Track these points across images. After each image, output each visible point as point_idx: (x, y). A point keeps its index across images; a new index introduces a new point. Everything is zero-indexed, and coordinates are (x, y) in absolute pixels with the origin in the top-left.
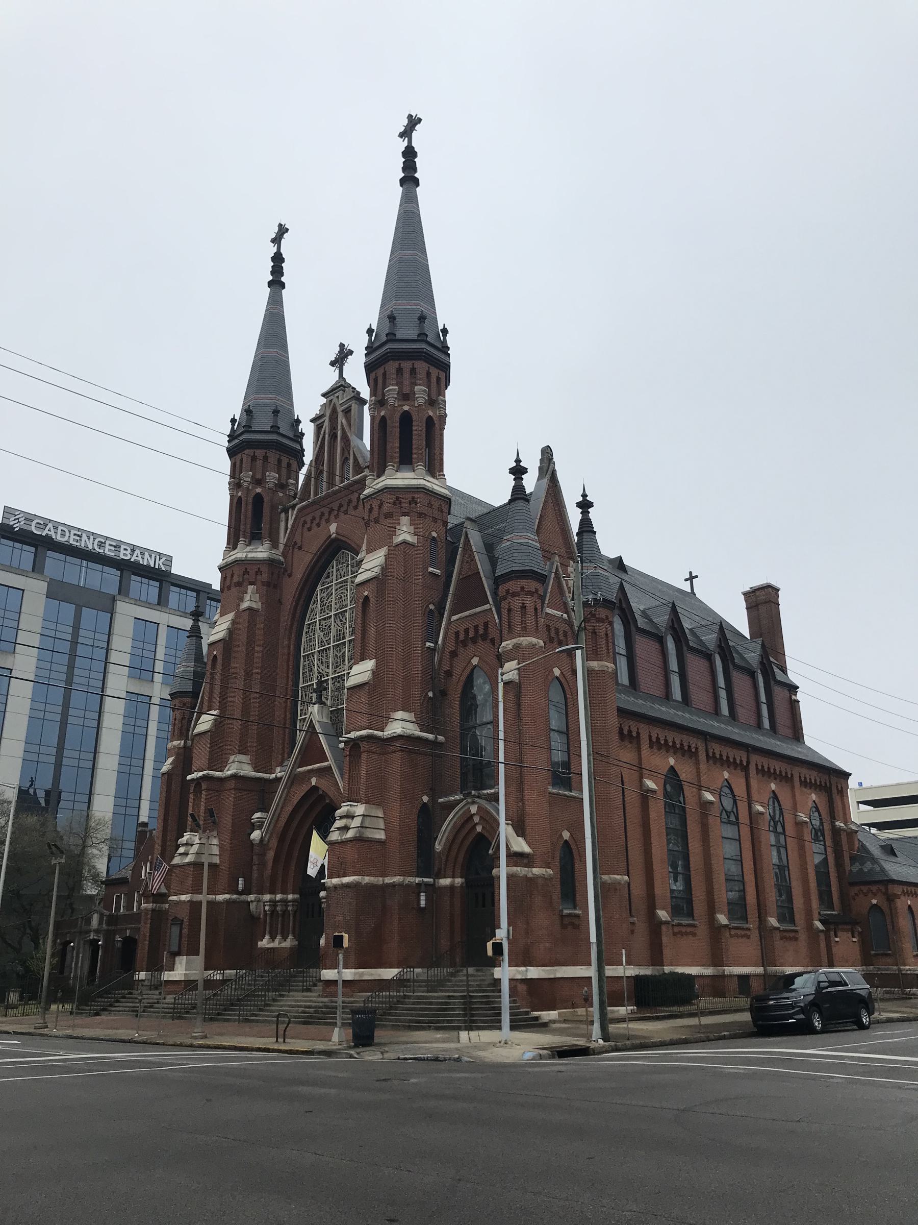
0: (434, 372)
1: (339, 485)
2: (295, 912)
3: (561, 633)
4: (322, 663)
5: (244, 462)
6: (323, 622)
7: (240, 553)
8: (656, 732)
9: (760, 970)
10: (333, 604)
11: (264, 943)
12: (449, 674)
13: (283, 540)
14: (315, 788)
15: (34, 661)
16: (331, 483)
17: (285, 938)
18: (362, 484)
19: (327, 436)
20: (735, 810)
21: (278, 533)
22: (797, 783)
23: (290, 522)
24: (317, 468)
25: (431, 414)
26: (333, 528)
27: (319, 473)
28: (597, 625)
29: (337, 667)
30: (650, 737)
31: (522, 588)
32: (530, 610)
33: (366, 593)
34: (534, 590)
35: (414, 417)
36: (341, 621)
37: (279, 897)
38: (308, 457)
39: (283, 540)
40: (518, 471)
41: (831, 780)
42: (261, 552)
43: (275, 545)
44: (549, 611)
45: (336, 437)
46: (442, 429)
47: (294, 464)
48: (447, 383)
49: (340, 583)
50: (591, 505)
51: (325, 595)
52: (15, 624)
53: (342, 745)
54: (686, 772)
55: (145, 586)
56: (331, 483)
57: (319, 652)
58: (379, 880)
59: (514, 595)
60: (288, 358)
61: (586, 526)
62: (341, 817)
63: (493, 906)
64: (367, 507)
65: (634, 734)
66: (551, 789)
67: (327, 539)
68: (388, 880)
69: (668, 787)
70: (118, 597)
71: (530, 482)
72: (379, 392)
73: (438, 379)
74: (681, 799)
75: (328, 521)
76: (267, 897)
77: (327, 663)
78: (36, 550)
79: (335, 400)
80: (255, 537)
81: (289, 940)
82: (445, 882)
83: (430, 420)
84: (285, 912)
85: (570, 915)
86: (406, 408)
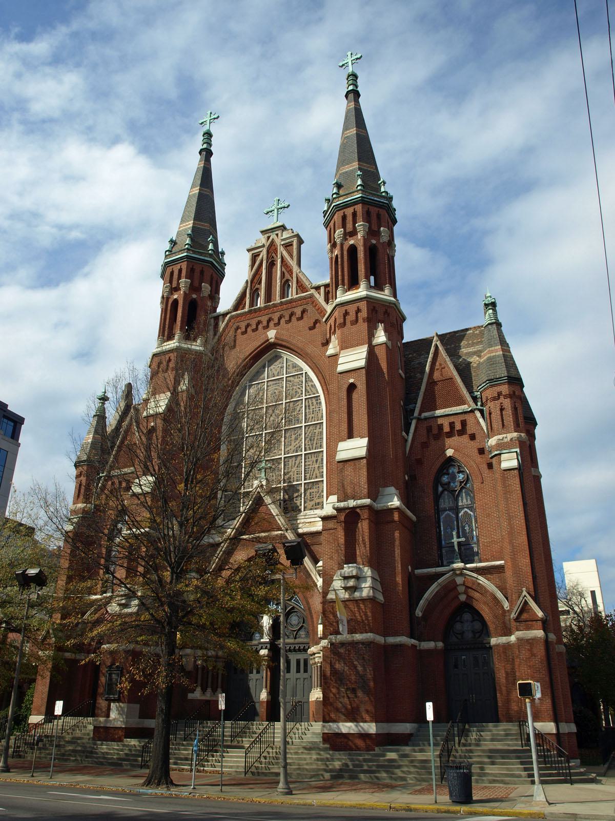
26: (272, 334)
33: (351, 381)
56: (283, 294)
68: (392, 640)
75: (267, 327)
82: (430, 645)
86: (194, 296)
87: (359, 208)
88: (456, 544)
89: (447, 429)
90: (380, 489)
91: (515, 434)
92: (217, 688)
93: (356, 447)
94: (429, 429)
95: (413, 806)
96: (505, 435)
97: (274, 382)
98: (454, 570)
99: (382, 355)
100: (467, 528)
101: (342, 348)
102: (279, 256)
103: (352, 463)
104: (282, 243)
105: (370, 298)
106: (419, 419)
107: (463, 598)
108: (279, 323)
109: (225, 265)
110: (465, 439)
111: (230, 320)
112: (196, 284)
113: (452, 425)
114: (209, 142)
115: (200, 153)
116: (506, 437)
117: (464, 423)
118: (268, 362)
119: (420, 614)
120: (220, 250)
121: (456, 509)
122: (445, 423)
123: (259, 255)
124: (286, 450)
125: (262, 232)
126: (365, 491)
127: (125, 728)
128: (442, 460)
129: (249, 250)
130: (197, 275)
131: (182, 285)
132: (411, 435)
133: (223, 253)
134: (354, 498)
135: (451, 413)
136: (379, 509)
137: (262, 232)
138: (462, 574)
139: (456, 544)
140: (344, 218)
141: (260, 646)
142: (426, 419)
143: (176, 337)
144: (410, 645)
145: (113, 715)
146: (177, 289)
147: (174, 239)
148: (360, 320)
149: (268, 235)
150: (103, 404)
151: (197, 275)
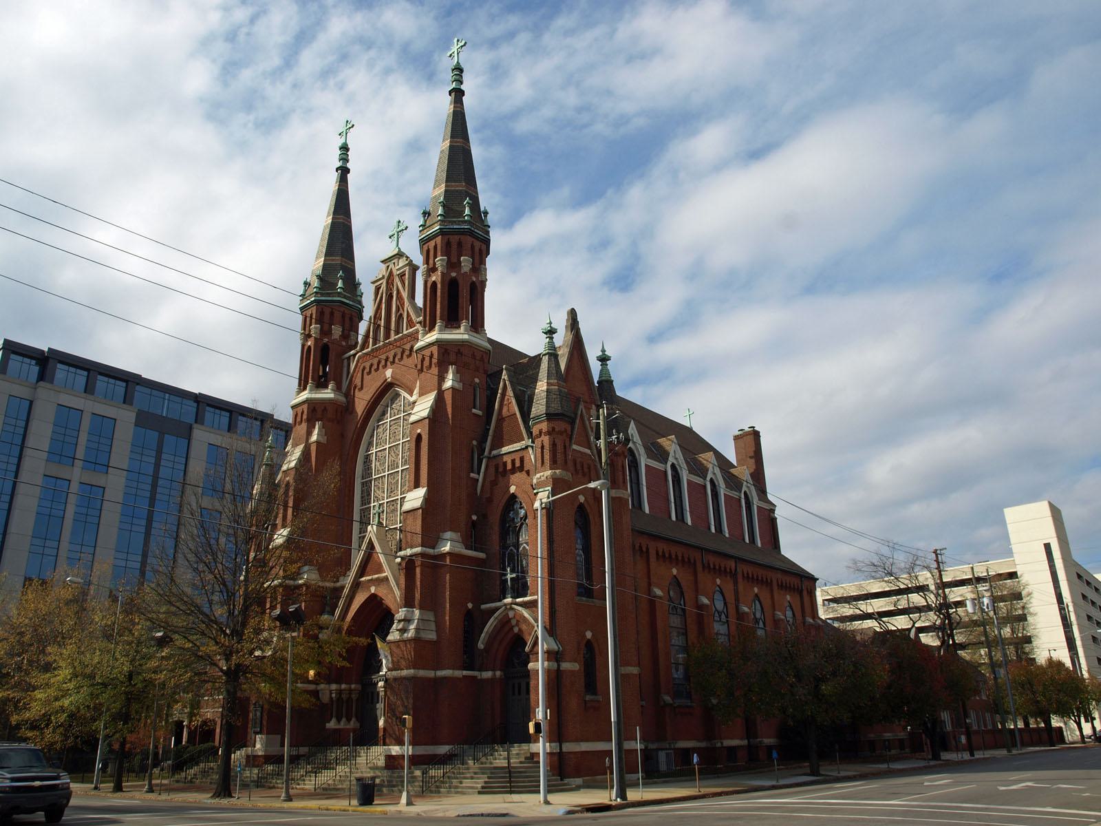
0: (477, 244)
2: (357, 700)
3: (585, 466)
4: (379, 488)
8: (662, 546)
9: (745, 742)
11: (332, 724)
12: (490, 500)
14: (374, 596)
15: (124, 480)
17: (349, 720)
18: (414, 337)
19: (384, 295)
20: (725, 611)
22: (775, 587)
25: (474, 279)
26: (389, 373)
27: (377, 328)
33: (419, 431)
35: (460, 282)
37: (343, 686)
40: (551, 332)
41: (803, 583)
42: (328, 394)
44: (575, 447)
45: (392, 297)
46: (483, 291)
48: (488, 253)
49: (394, 420)
50: (608, 359)
53: (399, 560)
55: (217, 417)
56: (387, 336)
58: (430, 674)
60: (470, 147)
61: (604, 371)
63: (528, 692)
64: (420, 357)
65: (644, 549)
67: (384, 382)
68: (441, 673)
69: (671, 593)
70: (195, 426)
71: (561, 339)
72: (431, 262)
74: (682, 603)
75: (385, 366)
76: (334, 687)
77: (384, 489)
78: (127, 385)
79: (392, 266)
80: (321, 384)
81: (352, 723)
82: (487, 675)
83: (473, 284)
85: (592, 701)
86: (454, 274)
87: (439, 239)
88: (509, 579)
89: (509, 467)
90: (441, 534)
91: (549, 473)
93: (415, 498)
94: (497, 467)
95: (330, 807)
96: (542, 474)
97: (394, 422)
98: (505, 605)
99: (448, 397)
100: (524, 562)
101: (420, 396)
102: (395, 287)
103: (412, 513)
104: (398, 272)
105: (441, 342)
106: (489, 458)
107: (516, 630)
108: (393, 362)
109: (489, 227)
110: (524, 474)
111: (358, 361)
112: (454, 260)
113: (513, 461)
114: (460, 79)
115: (337, 170)
116: (543, 476)
117: (522, 460)
118: (391, 400)
120: (482, 209)
121: (517, 545)
122: (508, 459)
123: (380, 287)
124: (403, 490)
125: (382, 262)
126: (420, 540)
127: (265, 755)
128: (507, 497)
129: (373, 283)
130: (327, 317)
131: (438, 264)
132: (482, 474)
133: (486, 213)
134: (412, 547)
135: (514, 449)
136: (436, 554)
137: (382, 262)
138: (512, 609)
139: (509, 579)
141: (379, 679)
142: (495, 457)
143: (437, 328)
145: (258, 746)
146: (309, 336)
147: (308, 281)
148: (433, 366)
149: (387, 265)
150: (551, 338)
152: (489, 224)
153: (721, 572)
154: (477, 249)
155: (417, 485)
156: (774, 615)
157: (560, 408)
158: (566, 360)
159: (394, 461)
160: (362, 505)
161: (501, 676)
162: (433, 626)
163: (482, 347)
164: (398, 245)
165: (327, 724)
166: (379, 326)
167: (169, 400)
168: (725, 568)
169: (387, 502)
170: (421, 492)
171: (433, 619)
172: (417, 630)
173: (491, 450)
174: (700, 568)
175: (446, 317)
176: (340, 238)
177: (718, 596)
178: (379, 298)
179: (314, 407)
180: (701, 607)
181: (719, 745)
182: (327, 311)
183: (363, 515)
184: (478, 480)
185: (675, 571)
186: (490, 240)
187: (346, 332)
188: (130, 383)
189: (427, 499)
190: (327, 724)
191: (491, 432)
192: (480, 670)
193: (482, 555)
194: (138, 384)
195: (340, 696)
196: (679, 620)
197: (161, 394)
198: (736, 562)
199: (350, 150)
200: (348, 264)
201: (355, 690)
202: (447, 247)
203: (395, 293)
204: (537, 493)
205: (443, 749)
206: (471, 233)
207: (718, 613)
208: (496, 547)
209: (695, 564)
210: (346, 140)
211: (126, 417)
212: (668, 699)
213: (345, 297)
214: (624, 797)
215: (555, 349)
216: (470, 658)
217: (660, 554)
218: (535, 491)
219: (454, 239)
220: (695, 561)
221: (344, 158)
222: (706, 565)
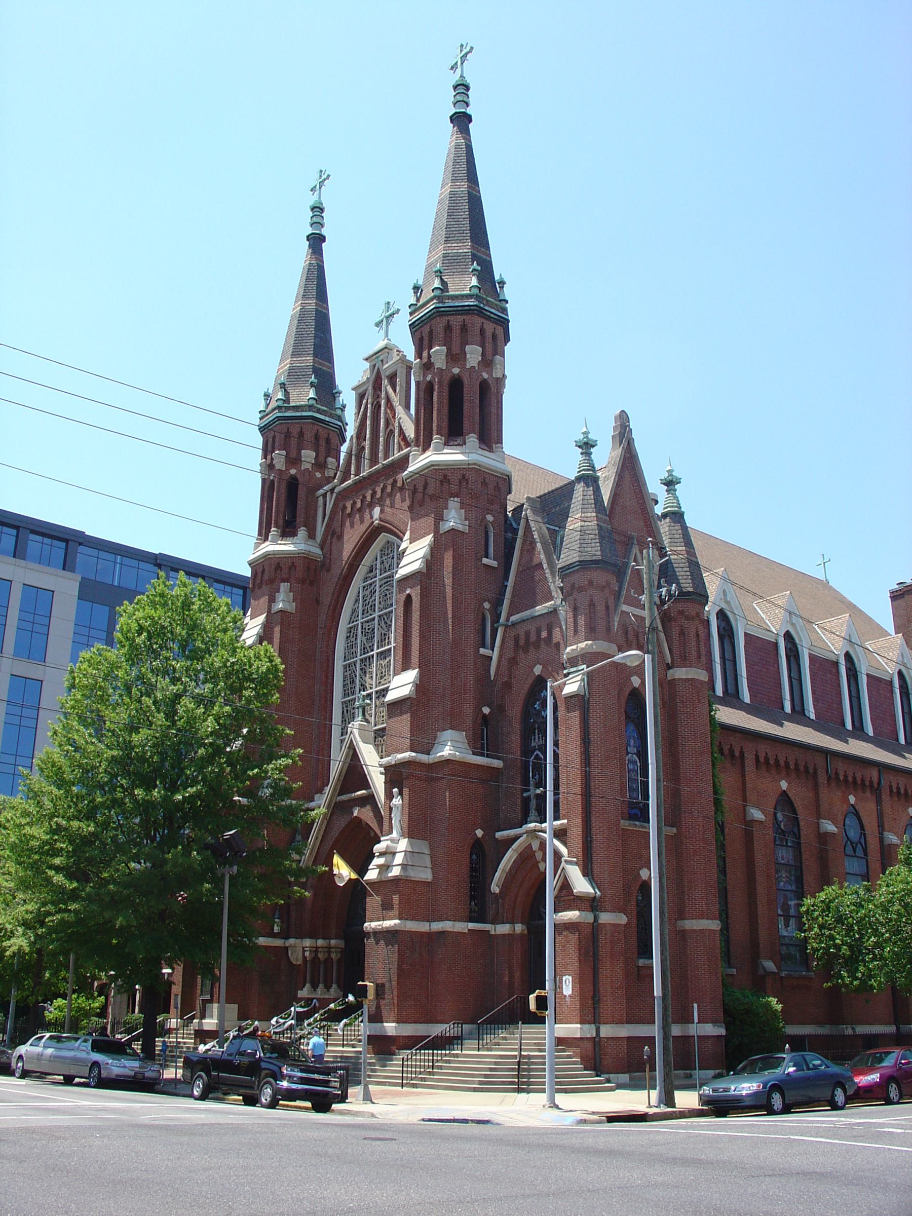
0: (489, 327)
1: (383, 462)
2: (339, 961)
5: (277, 440)
6: (366, 625)
7: (269, 547)
10: (377, 603)
12: (508, 685)
13: (320, 530)
16: (374, 460)
17: (328, 987)
18: (404, 462)
20: (863, 841)
21: (315, 521)
23: (329, 506)
24: (358, 444)
25: (485, 376)
28: (686, 623)
29: (381, 678)
30: (757, 756)
31: (591, 583)
32: (600, 608)
33: (408, 592)
34: (605, 584)
35: (466, 381)
36: (386, 623)
38: (351, 431)
39: (320, 530)
40: (586, 446)
43: (311, 535)
45: (380, 406)
47: (335, 439)
48: (507, 339)
51: (368, 592)
52: (46, 622)
54: (800, 796)
56: (374, 460)
57: (361, 660)
59: (581, 589)
60: (479, 192)
62: (382, 854)
65: (737, 754)
66: (624, 824)
68: (437, 926)
71: (605, 457)
72: (425, 354)
73: (494, 337)
75: (371, 506)
76: (307, 942)
81: (332, 990)
82: (503, 929)
84: (328, 960)
86: (456, 371)
92: (332, 983)
101: (411, 543)
106: (507, 627)
112: (456, 350)
114: (466, 99)
119: (497, 891)
120: (497, 278)
125: (367, 359)
128: (530, 681)
133: (502, 283)
136: (431, 762)
137: (367, 359)
140: (448, 328)
144: (466, 931)
151: (294, 441)
152: (507, 298)
153: (858, 786)
154: (489, 334)
155: (406, 667)
156: (881, 840)
157: (599, 553)
158: (611, 485)
159: (385, 635)
160: (345, 696)
161: (523, 930)
162: (428, 861)
163: (497, 472)
164: (387, 335)
165: (299, 992)
166: (363, 448)
167: (121, 564)
168: (863, 780)
169: (377, 692)
170: (411, 675)
171: (427, 851)
172: (404, 866)
173: (510, 614)
174: (822, 779)
175: (445, 431)
176: (314, 333)
177: (851, 821)
178: (362, 410)
179: (279, 564)
180: (824, 838)
181: (849, 1032)
182: (295, 432)
183: (345, 709)
184: (491, 658)
185: (784, 785)
186: (508, 321)
187: (321, 459)
188: (70, 542)
189: (420, 686)
190: (299, 992)
191: (509, 590)
192: (494, 922)
193: (497, 763)
194: (80, 544)
195: (316, 955)
196: (791, 854)
197: (111, 557)
198: (879, 771)
199: (326, 210)
200: (324, 365)
201: (322, 947)
202: (445, 332)
203: (383, 402)
204: (569, 674)
205: (437, 1030)
206: (478, 311)
207: (852, 843)
208: (517, 755)
209: (815, 774)
210: (320, 198)
211: (65, 588)
212: (770, 965)
213: (319, 411)
214: (669, 1100)
215: (593, 468)
216: (478, 904)
217: (762, 760)
218: (565, 672)
219: (456, 321)
220: (815, 769)
221: (317, 222)
222: (833, 776)
